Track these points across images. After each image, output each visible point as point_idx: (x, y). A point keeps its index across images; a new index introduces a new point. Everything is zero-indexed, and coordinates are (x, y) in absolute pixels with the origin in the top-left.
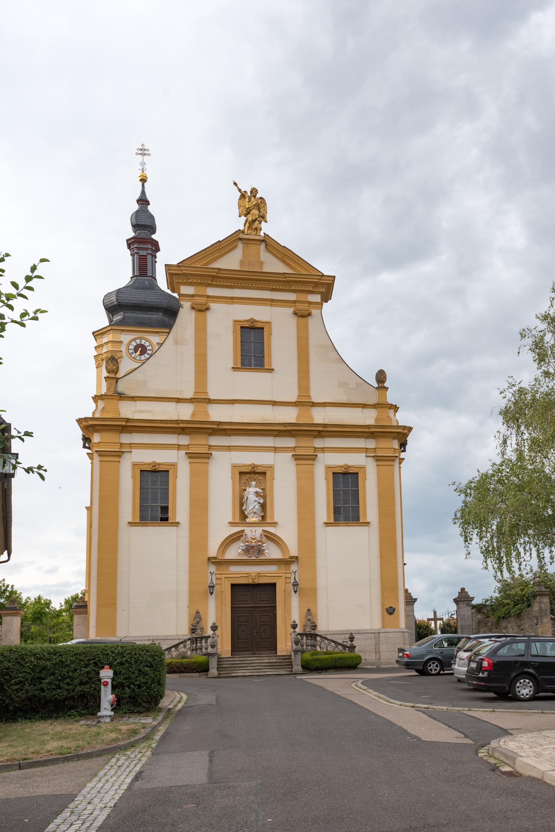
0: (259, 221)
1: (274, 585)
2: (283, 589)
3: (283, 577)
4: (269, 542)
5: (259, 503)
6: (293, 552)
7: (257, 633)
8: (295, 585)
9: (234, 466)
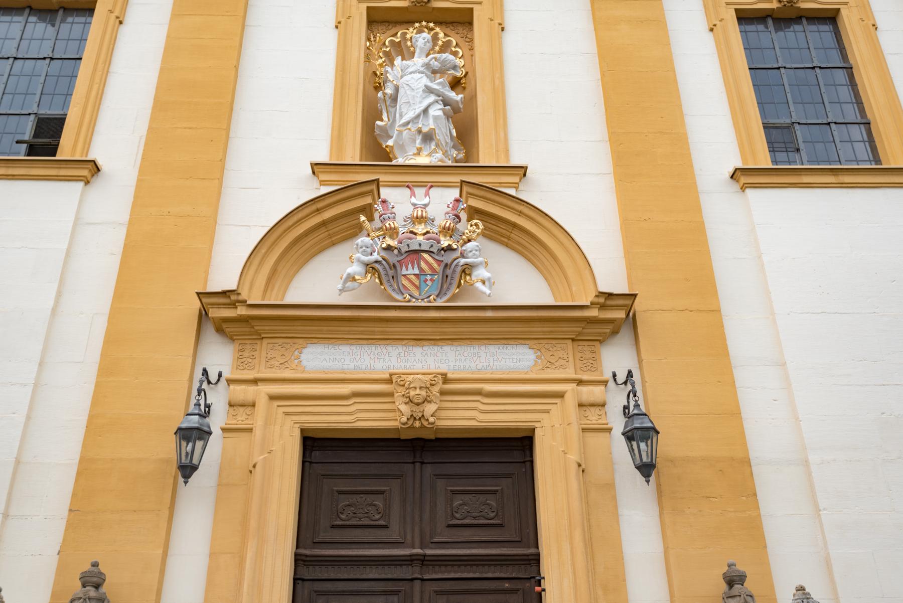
1: (518, 447)
2: (573, 457)
3: (570, 401)
4: (495, 251)
6: (611, 276)
8: (640, 433)
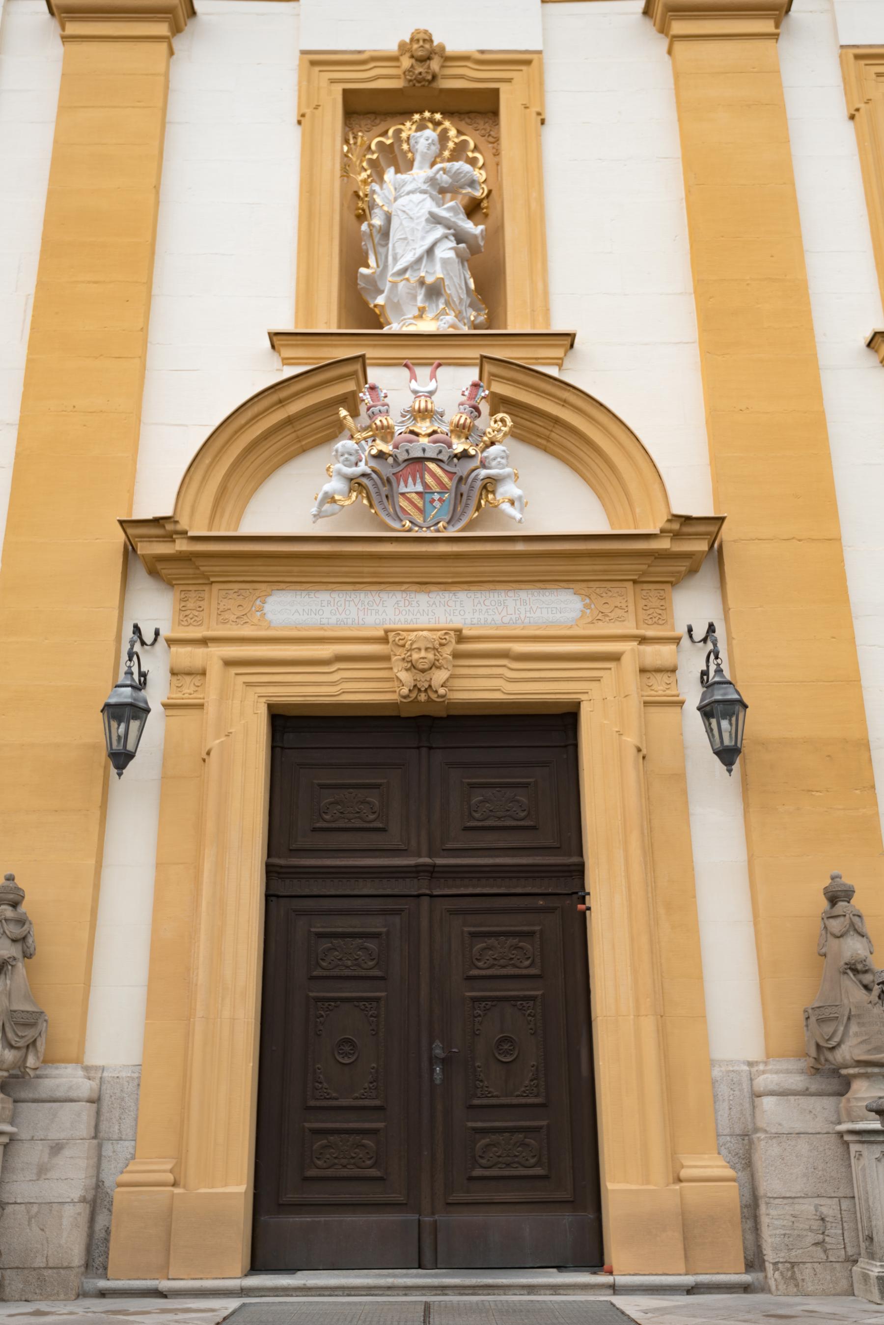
1: (557, 726)
2: (631, 739)
3: (629, 665)
5: (460, 237)
6: (691, 498)
7: (446, 1062)
9: (316, 61)
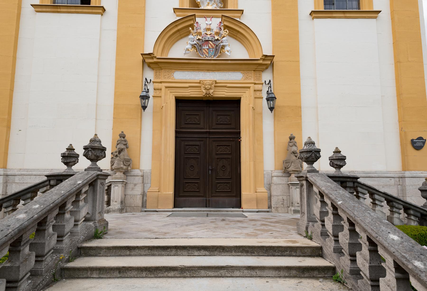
0: (209, 47)
1: (235, 103)
2: (251, 105)
3: (252, 89)
8: (271, 99)
